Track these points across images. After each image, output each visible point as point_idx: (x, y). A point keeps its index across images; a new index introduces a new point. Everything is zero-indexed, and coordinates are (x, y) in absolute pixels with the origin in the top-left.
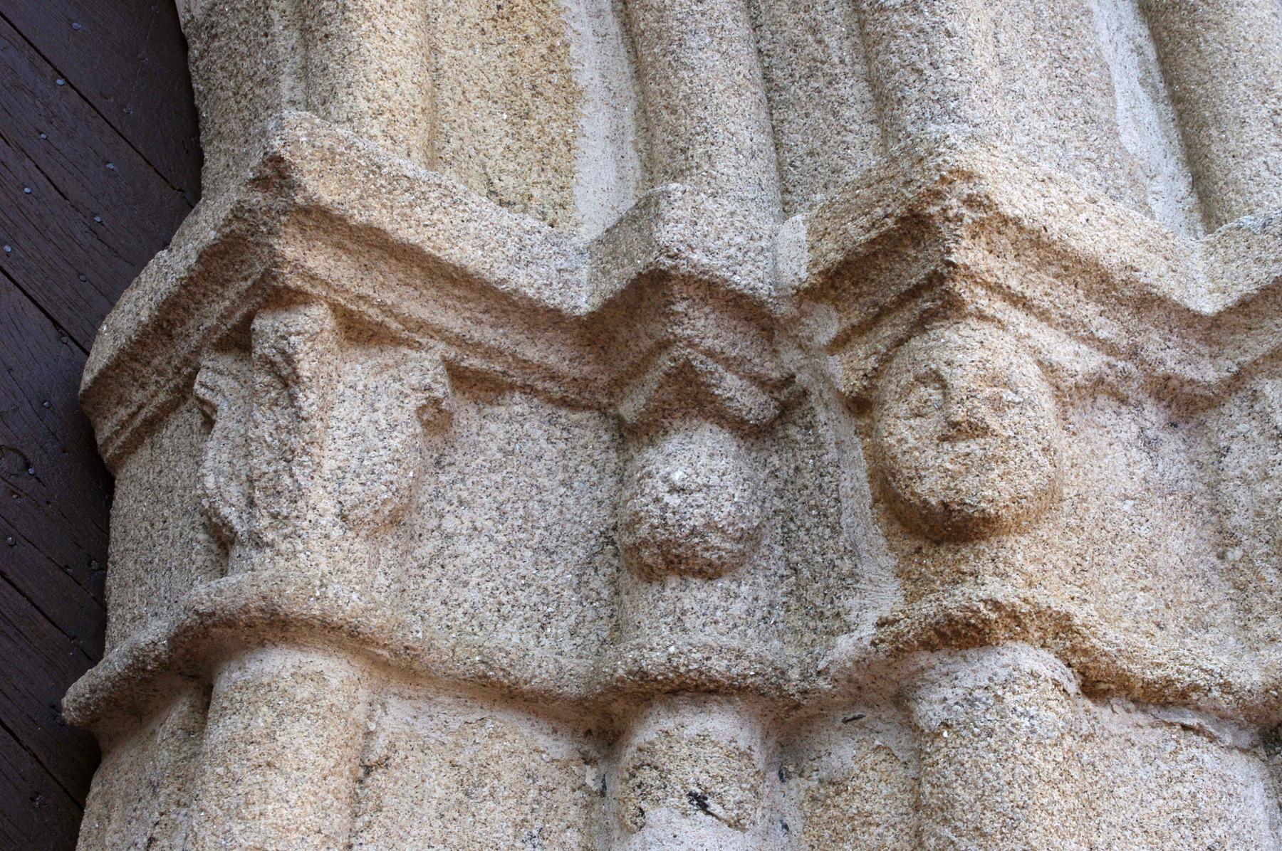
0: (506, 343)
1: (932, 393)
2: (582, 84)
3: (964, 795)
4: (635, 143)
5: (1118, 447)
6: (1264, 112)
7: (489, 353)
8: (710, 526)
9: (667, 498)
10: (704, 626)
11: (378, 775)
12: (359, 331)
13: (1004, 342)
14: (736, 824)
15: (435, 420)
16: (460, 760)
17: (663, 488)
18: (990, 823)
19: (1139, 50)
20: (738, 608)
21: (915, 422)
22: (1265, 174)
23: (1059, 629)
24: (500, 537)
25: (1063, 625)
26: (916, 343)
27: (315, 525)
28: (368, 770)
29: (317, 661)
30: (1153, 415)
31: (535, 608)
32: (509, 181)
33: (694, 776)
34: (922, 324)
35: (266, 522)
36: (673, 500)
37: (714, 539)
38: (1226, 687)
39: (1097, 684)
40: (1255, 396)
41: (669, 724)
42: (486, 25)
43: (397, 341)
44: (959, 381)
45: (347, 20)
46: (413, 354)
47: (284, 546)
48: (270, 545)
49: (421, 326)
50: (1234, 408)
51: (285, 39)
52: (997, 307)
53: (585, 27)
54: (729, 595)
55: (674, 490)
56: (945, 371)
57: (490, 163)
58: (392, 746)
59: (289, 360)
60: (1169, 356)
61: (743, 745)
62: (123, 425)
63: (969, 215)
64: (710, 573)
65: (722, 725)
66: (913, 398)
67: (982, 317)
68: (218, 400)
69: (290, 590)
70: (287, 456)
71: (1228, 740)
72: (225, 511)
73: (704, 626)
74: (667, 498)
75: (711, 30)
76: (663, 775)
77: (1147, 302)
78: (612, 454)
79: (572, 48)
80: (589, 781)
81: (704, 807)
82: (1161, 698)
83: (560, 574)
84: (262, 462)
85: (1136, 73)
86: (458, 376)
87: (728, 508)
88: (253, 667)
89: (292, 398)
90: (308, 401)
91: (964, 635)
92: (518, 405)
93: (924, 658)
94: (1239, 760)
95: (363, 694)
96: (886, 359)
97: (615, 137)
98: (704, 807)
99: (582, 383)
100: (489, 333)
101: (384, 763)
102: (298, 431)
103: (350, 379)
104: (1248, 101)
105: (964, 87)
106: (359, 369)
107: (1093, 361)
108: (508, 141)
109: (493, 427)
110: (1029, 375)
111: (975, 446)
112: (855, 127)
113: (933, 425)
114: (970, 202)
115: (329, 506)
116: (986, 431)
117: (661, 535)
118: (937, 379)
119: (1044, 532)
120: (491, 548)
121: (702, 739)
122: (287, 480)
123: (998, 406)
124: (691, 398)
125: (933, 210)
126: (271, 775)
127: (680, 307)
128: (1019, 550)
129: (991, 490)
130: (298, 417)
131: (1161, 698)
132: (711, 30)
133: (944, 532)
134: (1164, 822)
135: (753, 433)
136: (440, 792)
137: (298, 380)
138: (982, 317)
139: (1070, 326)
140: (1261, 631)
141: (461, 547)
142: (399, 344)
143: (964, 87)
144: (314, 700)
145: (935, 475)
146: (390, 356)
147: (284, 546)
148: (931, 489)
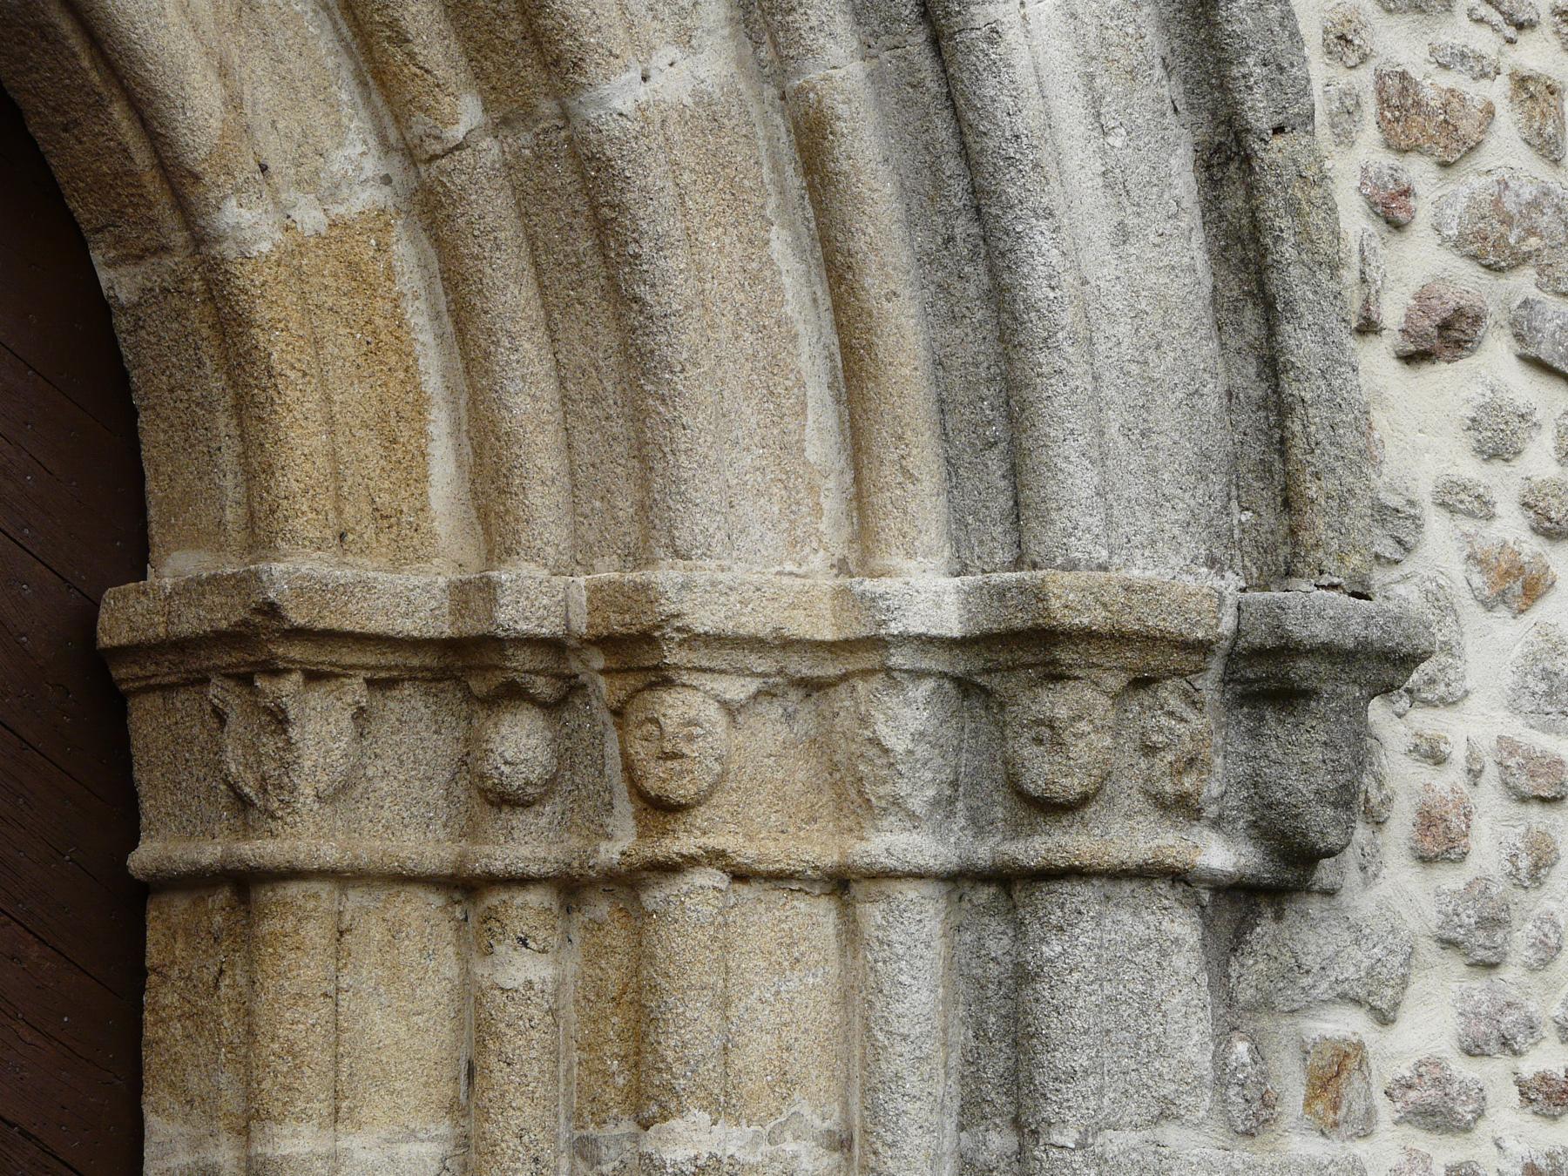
0: (400, 661)
1: (652, 728)
2: (429, 391)
3: (660, 953)
4: (468, 432)
5: (769, 724)
6: (895, 457)
7: (389, 669)
8: (528, 783)
9: (503, 768)
10: (524, 845)
11: (347, 936)
12: (314, 676)
13: (696, 698)
14: (544, 951)
15: (361, 714)
16: (387, 916)
17: (500, 760)
18: (672, 971)
19: (831, 357)
20: (543, 821)
21: (645, 744)
22: (890, 507)
23: (717, 857)
24: (401, 777)
25: (721, 854)
26: (646, 694)
27: (304, 804)
28: (342, 933)
29: (315, 886)
30: (794, 695)
31: (423, 816)
32: (386, 497)
33: (520, 928)
34: (651, 686)
35: (276, 805)
36: (506, 769)
37: (530, 790)
38: (816, 868)
39: (741, 876)
40: (854, 688)
41: (505, 897)
42: (359, 361)
43: (337, 676)
44: (670, 726)
45: (276, 412)
46: (347, 681)
47: (289, 819)
48: (281, 818)
49: (352, 667)
50: (843, 689)
51: (224, 423)
52: (700, 658)
53: (427, 337)
54: (539, 815)
55: (506, 763)
56: (662, 719)
57: (372, 484)
58: (353, 918)
59: (283, 711)
60: (803, 666)
61: (546, 905)
62: (138, 678)
63: (678, 636)
64: (527, 805)
65: (535, 897)
66: (644, 729)
67: (684, 685)
68: (227, 710)
69: (302, 857)
70: (286, 766)
71: (817, 892)
72: (247, 790)
73: (524, 845)
74: (503, 768)
75: (523, 377)
76: (503, 927)
77: (788, 644)
78: (464, 705)
79: (421, 360)
80: (457, 914)
81: (526, 945)
82: (779, 878)
83: (435, 792)
84: (270, 767)
85: (825, 379)
86: (370, 683)
87: (539, 770)
88: (280, 892)
89: (285, 731)
90: (294, 733)
91: (670, 868)
92: (408, 689)
93: (645, 874)
94: (824, 901)
95: (336, 894)
96: (631, 697)
97: (455, 432)
98: (526, 945)
99: (443, 670)
100: (390, 657)
101: (349, 930)
102: (291, 751)
103: (312, 703)
104: (886, 446)
105: (691, 473)
106: (317, 698)
107: (753, 685)
108: (383, 463)
109: (392, 705)
110: (712, 711)
111: (675, 764)
112: (623, 461)
113: (653, 748)
114: (678, 630)
115: (309, 791)
116: (683, 756)
117: (499, 789)
118: (656, 721)
119: (714, 802)
120: (396, 784)
121: (524, 906)
122: (286, 780)
123: (691, 739)
124: (513, 694)
125: (657, 634)
126: (299, 953)
127: (510, 652)
128: (700, 817)
129: (681, 790)
130: (288, 741)
131: (779, 878)
132: (523, 377)
133: (660, 809)
134: (774, 945)
135: (552, 708)
136: (378, 937)
137: (288, 721)
138: (684, 685)
139: (741, 672)
140: (846, 823)
141: (378, 784)
142: (455, 1109)
143: (691, 473)
144: (315, 910)
145: (656, 777)
146: (333, 685)
147: (289, 819)
148: (652, 786)
